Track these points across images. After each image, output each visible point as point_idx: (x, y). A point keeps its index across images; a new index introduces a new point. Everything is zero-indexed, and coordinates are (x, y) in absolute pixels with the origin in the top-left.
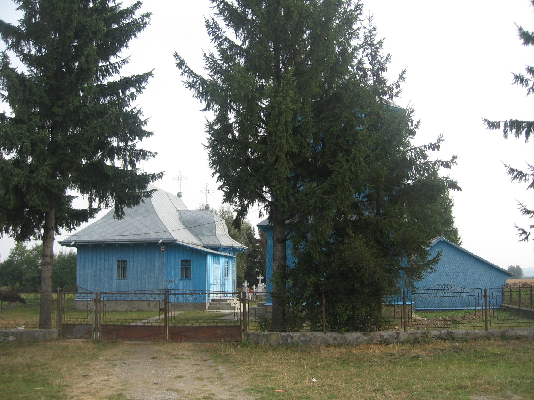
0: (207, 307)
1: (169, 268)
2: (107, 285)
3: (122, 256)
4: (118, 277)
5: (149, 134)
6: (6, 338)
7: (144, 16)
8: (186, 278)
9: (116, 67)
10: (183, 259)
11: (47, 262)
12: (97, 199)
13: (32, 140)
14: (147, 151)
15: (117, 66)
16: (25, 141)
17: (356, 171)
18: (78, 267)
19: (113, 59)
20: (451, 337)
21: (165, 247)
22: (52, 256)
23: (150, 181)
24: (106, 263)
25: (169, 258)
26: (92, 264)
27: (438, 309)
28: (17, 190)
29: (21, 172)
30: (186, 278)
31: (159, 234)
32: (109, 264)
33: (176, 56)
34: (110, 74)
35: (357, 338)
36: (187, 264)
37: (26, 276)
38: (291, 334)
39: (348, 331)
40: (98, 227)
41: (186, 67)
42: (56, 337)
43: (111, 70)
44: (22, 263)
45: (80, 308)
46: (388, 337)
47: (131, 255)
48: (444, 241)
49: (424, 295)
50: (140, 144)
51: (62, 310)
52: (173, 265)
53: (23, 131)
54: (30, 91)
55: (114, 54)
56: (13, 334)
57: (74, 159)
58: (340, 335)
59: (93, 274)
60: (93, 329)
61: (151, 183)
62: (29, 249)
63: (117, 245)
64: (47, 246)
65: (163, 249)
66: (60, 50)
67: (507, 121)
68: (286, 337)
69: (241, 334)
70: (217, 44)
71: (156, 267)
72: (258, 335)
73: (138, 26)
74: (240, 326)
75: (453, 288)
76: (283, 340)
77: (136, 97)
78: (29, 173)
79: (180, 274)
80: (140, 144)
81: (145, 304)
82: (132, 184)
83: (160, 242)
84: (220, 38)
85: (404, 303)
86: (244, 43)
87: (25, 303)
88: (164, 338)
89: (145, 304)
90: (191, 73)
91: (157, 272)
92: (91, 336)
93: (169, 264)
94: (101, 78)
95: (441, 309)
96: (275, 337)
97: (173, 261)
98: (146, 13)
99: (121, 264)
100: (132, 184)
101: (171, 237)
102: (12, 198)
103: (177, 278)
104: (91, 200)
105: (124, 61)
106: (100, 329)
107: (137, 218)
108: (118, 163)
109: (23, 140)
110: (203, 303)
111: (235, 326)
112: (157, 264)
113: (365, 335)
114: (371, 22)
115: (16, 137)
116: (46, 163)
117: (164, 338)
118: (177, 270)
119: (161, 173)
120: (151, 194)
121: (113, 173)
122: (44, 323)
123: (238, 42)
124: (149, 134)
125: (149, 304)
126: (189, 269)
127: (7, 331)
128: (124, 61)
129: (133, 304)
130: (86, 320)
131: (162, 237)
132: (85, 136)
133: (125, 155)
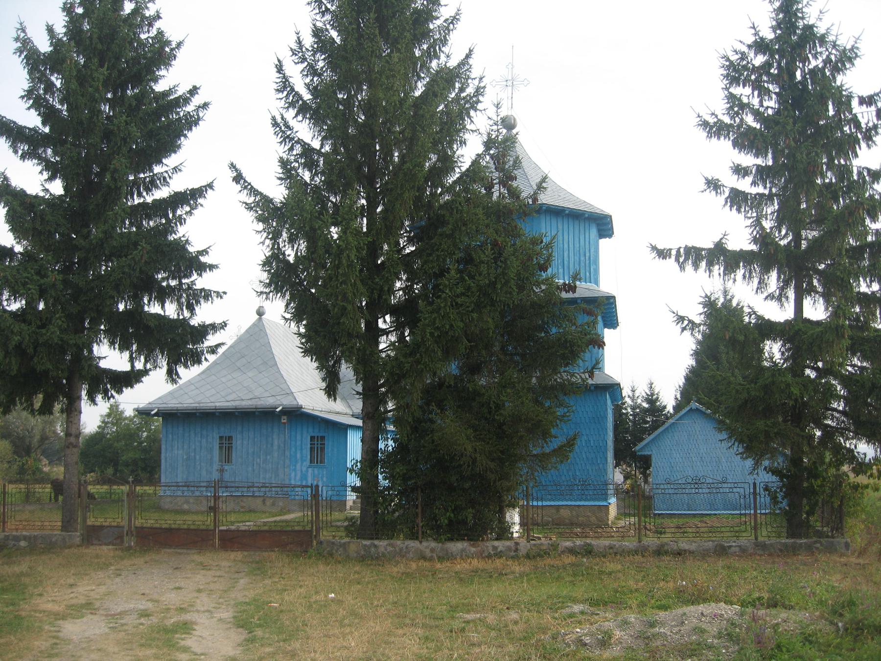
0: (348, 507)
1: (293, 449)
2: (204, 473)
3: (225, 431)
4: (221, 461)
5: (212, 267)
6: (16, 543)
7: (199, 107)
8: (317, 463)
9: (165, 178)
10: (313, 435)
11: (71, 444)
12: (142, 358)
13: (40, 286)
14: (210, 291)
15: (166, 175)
16: (31, 287)
17: (443, 326)
18: (163, 447)
19: (157, 169)
20: (588, 551)
21: (288, 418)
22: (79, 434)
23: (208, 334)
24: (204, 440)
25: (293, 433)
26: (183, 443)
27: (689, 512)
28: (20, 350)
29: (26, 328)
30: (317, 463)
31: (278, 398)
32: (207, 442)
33: (233, 166)
34: (157, 187)
35: (463, 550)
36: (319, 442)
37: (124, 458)
38: (376, 542)
39: (451, 539)
40: (193, 387)
41: (245, 181)
42: (78, 543)
43: (158, 182)
44: (118, 437)
45: (167, 507)
46: (503, 549)
47: (239, 428)
48: (697, 409)
49: (667, 491)
50: (202, 282)
51: (86, 507)
52: (299, 443)
53: (29, 275)
54: (42, 219)
55: (159, 162)
56: (25, 538)
57: (100, 308)
58: (440, 545)
59: (185, 457)
60: (125, 533)
61: (209, 337)
62: (128, 416)
63: (217, 414)
64: (71, 422)
65: (284, 419)
66: (81, 163)
67: (680, 248)
68: (369, 547)
69: (312, 542)
70: (287, 148)
71: (275, 448)
72: (333, 543)
73: (192, 122)
74: (311, 531)
75: (708, 482)
76: (365, 550)
77: (185, 220)
78: (39, 327)
79: (309, 457)
80: (202, 282)
81: (259, 501)
82: (182, 339)
83: (278, 410)
84: (292, 139)
85: (528, 503)
86: (322, 146)
87: (95, 499)
88: (213, 546)
89: (259, 501)
90: (253, 191)
91: (276, 454)
92: (122, 542)
93: (293, 443)
94: (145, 194)
95: (693, 512)
96: (356, 546)
97: (299, 437)
98: (203, 102)
99: (224, 442)
100: (182, 339)
101: (295, 403)
102: (14, 362)
103: (304, 463)
104: (132, 360)
105: (176, 169)
106: (134, 533)
107: (250, 374)
108: (171, 310)
109: (28, 286)
110: (342, 501)
111: (304, 531)
112: (276, 443)
113: (473, 546)
114: (499, 111)
115: (19, 283)
116: (57, 316)
117: (213, 546)
118: (304, 452)
119: (224, 322)
120: (217, 349)
121: (157, 323)
122: (67, 525)
123: (316, 145)
124: (212, 267)
125: (264, 502)
126: (323, 449)
127: (18, 534)
128: (176, 169)
129: (242, 501)
130: (117, 520)
131: (280, 402)
132: (112, 279)
133: (181, 296)
